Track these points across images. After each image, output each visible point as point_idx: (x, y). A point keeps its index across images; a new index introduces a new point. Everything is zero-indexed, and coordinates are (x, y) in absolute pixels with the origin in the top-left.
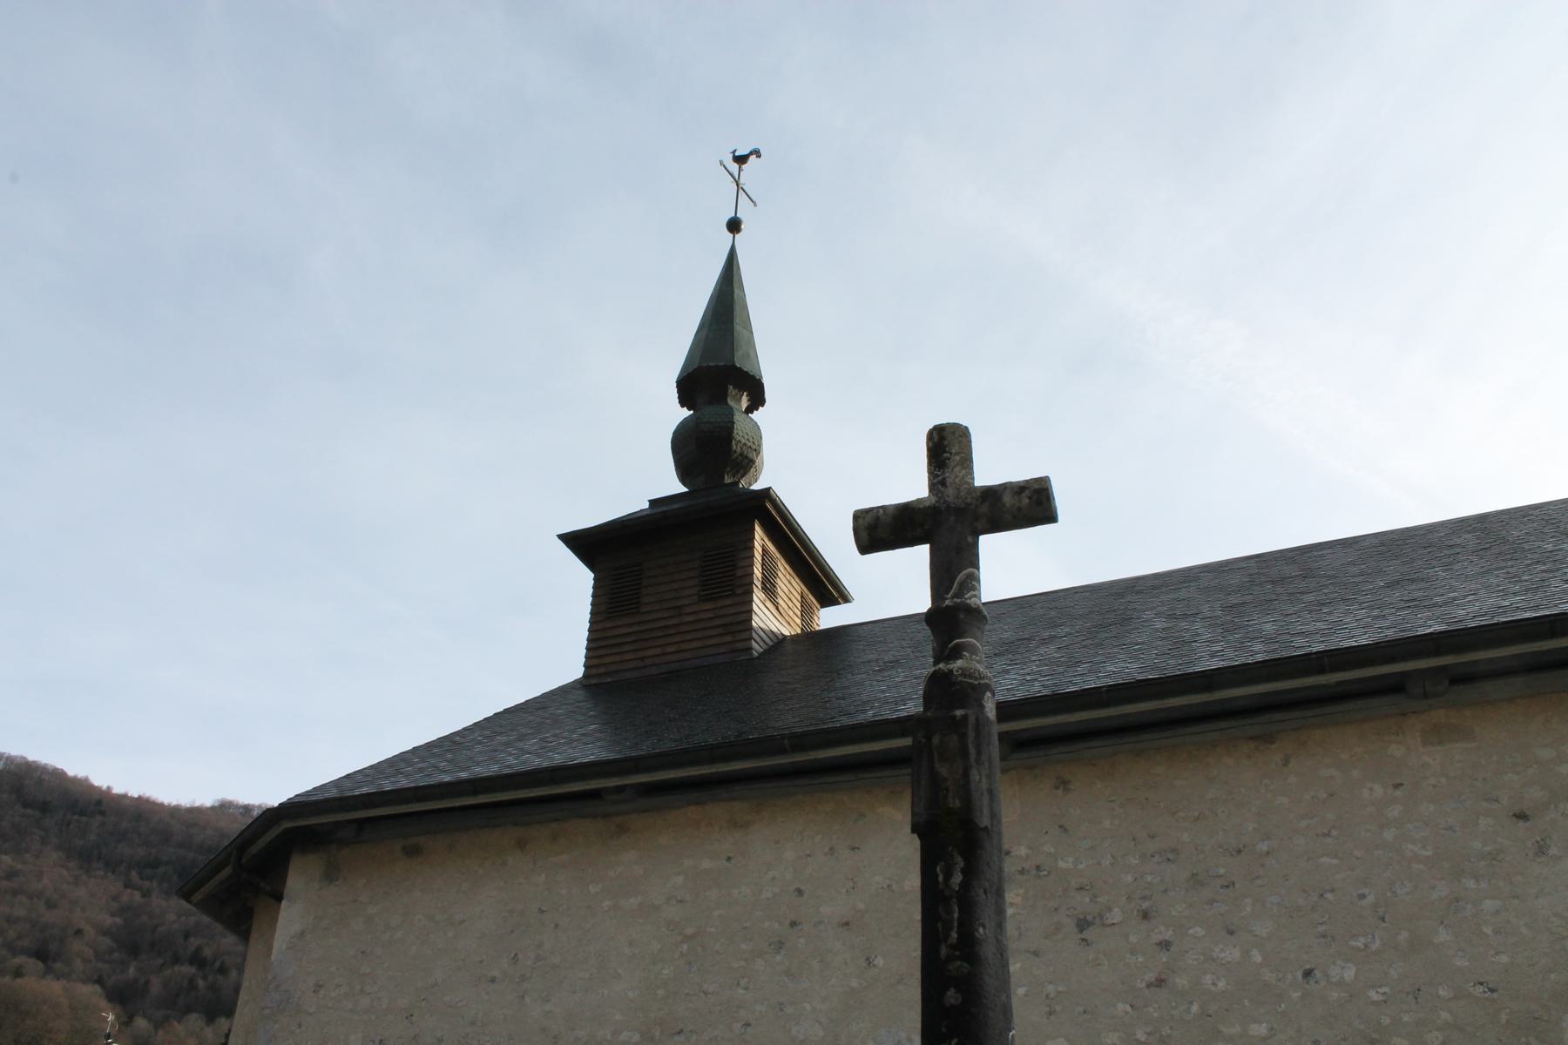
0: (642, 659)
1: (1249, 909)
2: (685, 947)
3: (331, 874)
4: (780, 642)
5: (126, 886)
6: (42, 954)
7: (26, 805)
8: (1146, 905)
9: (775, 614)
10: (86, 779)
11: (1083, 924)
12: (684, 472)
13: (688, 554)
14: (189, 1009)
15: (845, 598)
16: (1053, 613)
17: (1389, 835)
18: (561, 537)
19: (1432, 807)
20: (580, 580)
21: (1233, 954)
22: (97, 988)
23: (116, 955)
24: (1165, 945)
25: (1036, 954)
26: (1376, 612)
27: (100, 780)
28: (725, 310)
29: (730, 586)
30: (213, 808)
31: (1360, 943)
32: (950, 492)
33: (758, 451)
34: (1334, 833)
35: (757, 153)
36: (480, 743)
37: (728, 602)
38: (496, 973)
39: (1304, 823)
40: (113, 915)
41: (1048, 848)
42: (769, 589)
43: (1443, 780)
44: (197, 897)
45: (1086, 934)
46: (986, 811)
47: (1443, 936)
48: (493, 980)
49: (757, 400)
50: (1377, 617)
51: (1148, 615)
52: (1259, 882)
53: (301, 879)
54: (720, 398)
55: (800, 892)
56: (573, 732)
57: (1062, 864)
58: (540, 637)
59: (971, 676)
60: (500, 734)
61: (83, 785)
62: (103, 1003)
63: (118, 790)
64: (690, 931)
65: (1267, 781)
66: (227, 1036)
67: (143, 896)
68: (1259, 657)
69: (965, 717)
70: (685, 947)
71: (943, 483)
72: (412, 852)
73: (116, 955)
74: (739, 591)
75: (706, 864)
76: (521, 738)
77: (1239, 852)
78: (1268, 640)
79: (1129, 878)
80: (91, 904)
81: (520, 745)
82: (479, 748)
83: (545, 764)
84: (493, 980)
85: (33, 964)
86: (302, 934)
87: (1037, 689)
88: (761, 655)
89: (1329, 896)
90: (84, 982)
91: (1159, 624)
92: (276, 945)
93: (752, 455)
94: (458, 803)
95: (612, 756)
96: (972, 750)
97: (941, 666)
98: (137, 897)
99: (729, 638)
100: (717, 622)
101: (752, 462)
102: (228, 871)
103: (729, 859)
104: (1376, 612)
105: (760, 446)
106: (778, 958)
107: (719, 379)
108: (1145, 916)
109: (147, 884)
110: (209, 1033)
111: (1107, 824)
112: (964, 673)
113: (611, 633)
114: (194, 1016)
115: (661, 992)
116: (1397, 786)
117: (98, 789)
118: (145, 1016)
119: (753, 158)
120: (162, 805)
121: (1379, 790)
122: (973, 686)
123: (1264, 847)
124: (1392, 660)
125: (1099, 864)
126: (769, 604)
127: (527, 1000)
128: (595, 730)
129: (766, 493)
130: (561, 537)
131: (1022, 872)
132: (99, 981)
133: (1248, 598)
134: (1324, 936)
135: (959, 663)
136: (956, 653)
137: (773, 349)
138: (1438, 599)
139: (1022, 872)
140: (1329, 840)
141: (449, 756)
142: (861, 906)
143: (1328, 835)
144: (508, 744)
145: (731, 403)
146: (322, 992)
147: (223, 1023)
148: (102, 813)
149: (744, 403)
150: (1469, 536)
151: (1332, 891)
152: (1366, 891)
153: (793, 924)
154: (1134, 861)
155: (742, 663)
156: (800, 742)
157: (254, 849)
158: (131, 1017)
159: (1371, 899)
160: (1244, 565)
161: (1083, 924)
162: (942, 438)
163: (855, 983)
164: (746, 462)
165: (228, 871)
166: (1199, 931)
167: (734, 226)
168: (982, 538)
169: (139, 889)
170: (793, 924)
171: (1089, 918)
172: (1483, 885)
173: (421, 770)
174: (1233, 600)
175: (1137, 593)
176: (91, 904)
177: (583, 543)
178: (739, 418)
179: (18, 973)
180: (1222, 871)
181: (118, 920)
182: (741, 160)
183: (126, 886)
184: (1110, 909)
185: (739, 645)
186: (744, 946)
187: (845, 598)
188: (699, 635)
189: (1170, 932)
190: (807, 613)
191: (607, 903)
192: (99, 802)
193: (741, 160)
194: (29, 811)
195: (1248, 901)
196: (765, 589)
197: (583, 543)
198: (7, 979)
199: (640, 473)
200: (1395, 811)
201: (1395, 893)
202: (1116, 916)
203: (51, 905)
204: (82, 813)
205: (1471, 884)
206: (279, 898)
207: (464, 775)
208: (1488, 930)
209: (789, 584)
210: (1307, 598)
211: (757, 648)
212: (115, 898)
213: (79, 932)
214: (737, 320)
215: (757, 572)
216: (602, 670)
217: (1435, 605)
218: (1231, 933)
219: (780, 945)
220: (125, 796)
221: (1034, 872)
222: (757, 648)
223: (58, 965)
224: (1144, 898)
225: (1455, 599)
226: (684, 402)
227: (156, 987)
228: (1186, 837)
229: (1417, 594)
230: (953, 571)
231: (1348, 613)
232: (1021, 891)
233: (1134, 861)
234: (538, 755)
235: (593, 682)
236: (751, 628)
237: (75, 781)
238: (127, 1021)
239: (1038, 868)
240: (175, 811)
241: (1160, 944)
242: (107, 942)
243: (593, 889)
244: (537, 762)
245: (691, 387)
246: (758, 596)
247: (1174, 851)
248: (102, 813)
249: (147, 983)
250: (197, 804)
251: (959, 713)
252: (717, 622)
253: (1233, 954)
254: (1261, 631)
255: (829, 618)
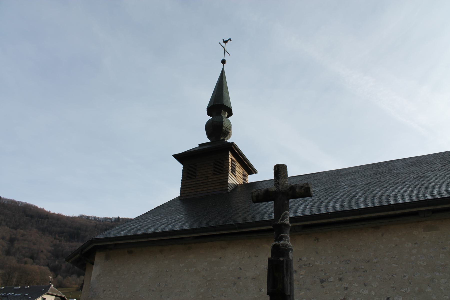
0: (197, 192)
1: (371, 279)
2: (208, 283)
3: (107, 258)
4: (236, 186)
5: (55, 239)
6: (32, 257)
7: (27, 216)
8: (341, 276)
9: (234, 180)
10: (43, 209)
11: (322, 281)
12: (209, 136)
13: (210, 161)
14: (73, 273)
15: (255, 172)
16: (316, 182)
17: (413, 258)
18: (174, 156)
19: (426, 250)
20: (179, 167)
21: (366, 292)
22: (47, 268)
23: (52, 258)
24: (346, 288)
25: (308, 289)
26: (410, 189)
27: (47, 209)
28: (223, 68)
29: (222, 171)
30: (78, 217)
31: (404, 290)
32: (280, 187)
33: (230, 129)
34: (396, 257)
35: (230, 40)
36: (149, 219)
37: (221, 175)
38: (154, 289)
39: (387, 254)
40: (51, 247)
41: (312, 258)
42: (233, 171)
43: (429, 242)
44: (70, 261)
45: (323, 284)
46: (289, 291)
47: (429, 289)
48: (153, 291)
49: (230, 114)
50: (410, 191)
51: (343, 184)
52: (374, 271)
53: (99, 259)
54: (220, 114)
55: (240, 269)
56: (176, 217)
57: (316, 263)
58: (167, 186)
59: (285, 247)
60: (155, 216)
61: (42, 210)
62: (49, 272)
63: (52, 212)
64: (209, 279)
65: (377, 241)
66: (83, 281)
67: (60, 241)
68: (375, 205)
69: (283, 261)
70: (208, 283)
71: (278, 183)
72: (130, 252)
73: (52, 258)
74: (225, 172)
75: (214, 259)
76: (161, 219)
77: (368, 261)
78: (378, 198)
79: (336, 268)
80: (45, 244)
81: (161, 221)
82: (149, 221)
83: (168, 230)
84: (153, 291)
85: (30, 260)
86: (100, 275)
87: (310, 212)
88: (231, 191)
89: (394, 276)
90: (44, 266)
91: (346, 189)
92: (92, 278)
93: (229, 131)
94: (143, 240)
95: (187, 228)
96: (285, 271)
97: (277, 242)
98: (58, 242)
99: (221, 186)
100: (218, 181)
101: (229, 133)
102: (78, 255)
103: (220, 258)
104: (410, 189)
105: (231, 128)
106: (234, 288)
107: (219, 107)
108: (340, 279)
109: (60, 238)
110: (78, 280)
111: (330, 252)
112: (283, 245)
113: (188, 184)
114: (74, 275)
115: (201, 296)
116: (416, 243)
117: (47, 211)
118: (61, 275)
119: (229, 41)
120: (64, 216)
121: (410, 244)
122: (286, 250)
123: (375, 260)
124: (415, 207)
125: (327, 264)
126: (233, 176)
127: (163, 297)
128: (182, 217)
129: (232, 144)
130: (174, 156)
131: (305, 265)
132: (48, 265)
133: (373, 180)
134: (393, 288)
135: (282, 242)
136: (281, 239)
137: (235, 98)
138: (429, 185)
139: (305, 265)
140: (395, 259)
141: (141, 224)
142: (258, 273)
143: (395, 257)
144: (157, 220)
145: (222, 115)
146: (105, 292)
147: (82, 277)
148: (48, 218)
149: (226, 115)
150: (439, 160)
151: (396, 274)
152: (406, 275)
153: (239, 278)
154: (337, 263)
155: (225, 194)
156: (241, 226)
157: (85, 250)
158: (57, 276)
159: (407, 277)
160: (371, 167)
161: (322, 281)
162: (278, 169)
163: (256, 296)
164: (227, 133)
165: (78, 255)
166: (356, 285)
167: (223, 62)
168: (290, 200)
169: (59, 240)
170: (239, 278)
171: (324, 279)
172: (441, 274)
173: (132, 229)
174: (369, 181)
175: (340, 175)
176: (45, 244)
177: (179, 157)
178: (225, 120)
179: (26, 263)
180: (363, 267)
181: (53, 248)
182: (225, 42)
183: (55, 239)
184: (330, 277)
185: (224, 188)
186: (224, 284)
187: (255, 172)
188: (213, 185)
189: (348, 285)
190: (244, 177)
191: (185, 270)
192: (47, 215)
193: (225, 42)
194: (28, 218)
195: (371, 276)
196: (232, 171)
197: (179, 157)
198: (23, 265)
199: (196, 137)
200: (415, 251)
201: (414, 276)
202: (332, 279)
203: (34, 244)
204: (42, 218)
205: (437, 274)
206: (93, 264)
207: (144, 232)
208: (442, 288)
209: (239, 169)
210: (391, 181)
211: (230, 189)
212: (52, 242)
213: (42, 251)
214: (224, 90)
215: (230, 167)
216: (185, 195)
217: (428, 188)
218: (366, 286)
219: (235, 284)
220: (54, 214)
221: (308, 265)
222: (230, 189)
223: (37, 261)
224: (340, 274)
225: (434, 185)
226: (209, 114)
227: (63, 267)
228: (353, 256)
229: (423, 183)
230: (280, 210)
231: (402, 188)
232: (304, 271)
233: (337, 263)
234: (166, 226)
235: (182, 198)
236: (228, 183)
237: (40, 209)
238: (55, 277)
239: (309, 264)
240: (68, 218)
241: (345, 288)
242: (49, 254)
243: (181, 265)
244: (166, 229)
245: (210, 110)
246: (230, 174)
247: (349, 260)
248: (48, 218)
249: (61, 265)
250: (74, 216)
251: (281, 259)
252: (218, 181)
253: (366, 292)
254: (376, 194)
255: (251, 179)
